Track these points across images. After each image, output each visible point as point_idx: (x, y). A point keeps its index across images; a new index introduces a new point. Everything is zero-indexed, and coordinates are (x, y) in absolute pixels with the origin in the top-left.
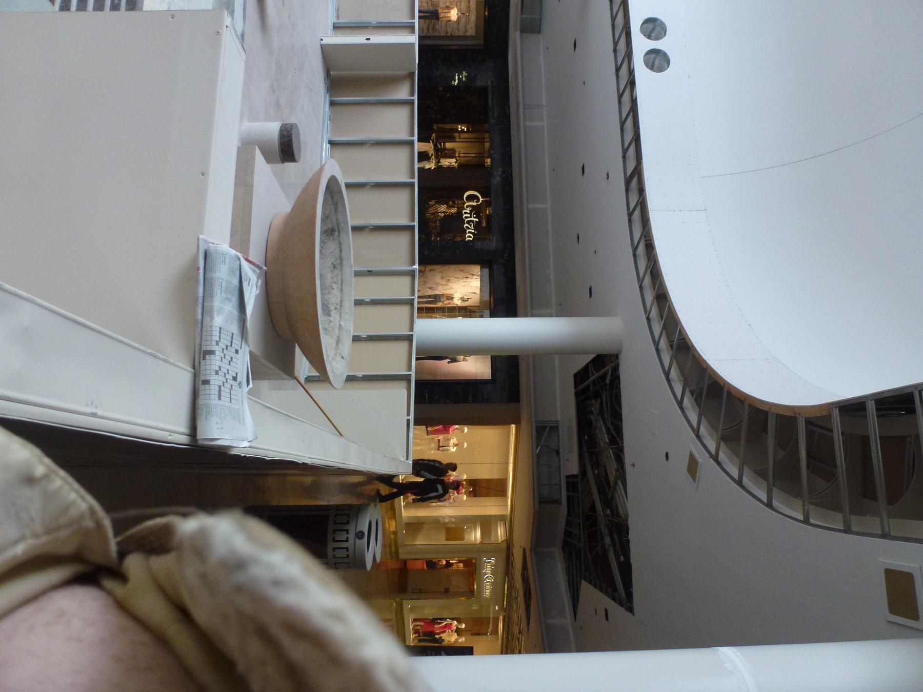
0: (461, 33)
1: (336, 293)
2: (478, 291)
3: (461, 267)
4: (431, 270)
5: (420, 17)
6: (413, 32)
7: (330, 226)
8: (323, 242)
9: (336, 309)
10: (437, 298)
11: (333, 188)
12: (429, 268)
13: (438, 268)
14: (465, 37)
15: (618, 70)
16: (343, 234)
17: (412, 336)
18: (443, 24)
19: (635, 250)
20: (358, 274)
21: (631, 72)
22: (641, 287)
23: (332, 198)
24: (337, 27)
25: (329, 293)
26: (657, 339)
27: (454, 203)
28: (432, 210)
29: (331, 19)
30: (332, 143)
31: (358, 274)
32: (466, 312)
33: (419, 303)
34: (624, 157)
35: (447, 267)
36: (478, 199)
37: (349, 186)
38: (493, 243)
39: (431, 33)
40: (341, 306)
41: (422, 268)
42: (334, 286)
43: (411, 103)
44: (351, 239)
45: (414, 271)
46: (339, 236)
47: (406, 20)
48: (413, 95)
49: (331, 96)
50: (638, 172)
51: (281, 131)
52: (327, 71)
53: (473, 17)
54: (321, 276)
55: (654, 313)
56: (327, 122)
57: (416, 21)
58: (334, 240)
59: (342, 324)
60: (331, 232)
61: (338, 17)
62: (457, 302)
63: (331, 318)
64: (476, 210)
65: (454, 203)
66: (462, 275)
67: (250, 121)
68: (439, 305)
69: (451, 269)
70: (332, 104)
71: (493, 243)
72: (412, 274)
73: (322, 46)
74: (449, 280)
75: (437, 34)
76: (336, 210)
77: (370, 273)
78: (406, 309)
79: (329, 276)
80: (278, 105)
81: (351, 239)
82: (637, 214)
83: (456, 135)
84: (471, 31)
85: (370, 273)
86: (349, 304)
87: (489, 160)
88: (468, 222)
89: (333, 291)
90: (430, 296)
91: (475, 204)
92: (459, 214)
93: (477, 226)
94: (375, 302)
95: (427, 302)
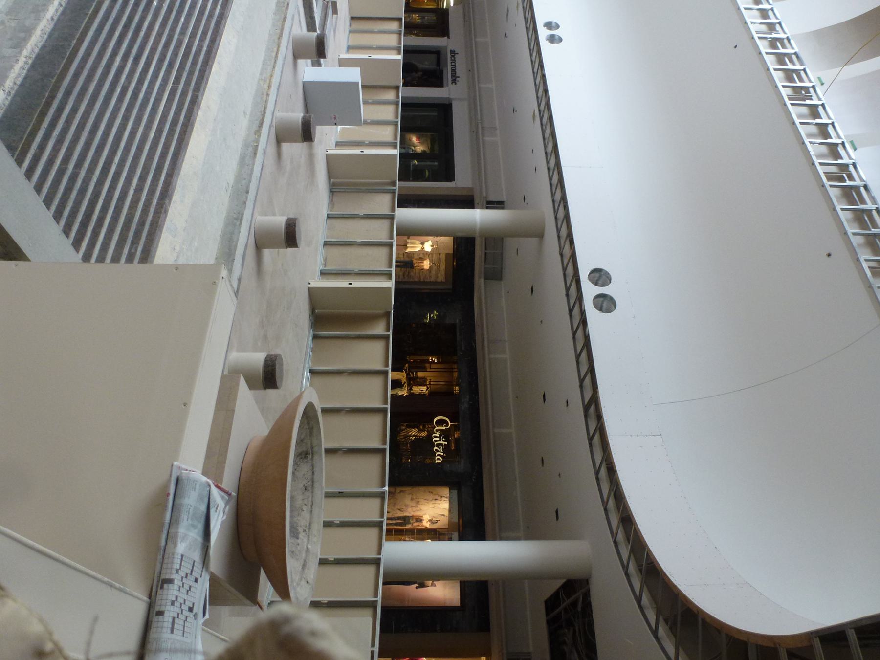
0: (432, 280)
1: (306, 515)
2: (447, 513)
3: (431, 489)
4: (401, 492)
5: (396, 266)
6: (390, 278)
7: (304, 449)
8: (296, 464)
9: (304, 531)
10: (406, 520)
11: (309, 414)
12: (399, 489)
13: (407, 489)
14: (435, 283)
15: (571, 311)
16: (316, 457)
17: (379, 559)
18: (417, 271)
19: (597, 473)
20: (328, 495)
21: (583, 313)
22: (606, 510)
23: (308, 424)
24: (323, 274)
25: (299, 515)
26: (614, 531)
27: (424, 427)
28: (403, 434)
29: (319, 267)
30: (312, 372)
31: (328, 495)
32: (436, 534)
33: (387, 524)
34: (581, 386)
35: (416, 489)
36: (447, 424)
37: (325, 411)
38: (462, 466)
39: (406, 279)
40: (310, 528)
41: (393, 490)
42: (305, 508)
43: (386, 338)
44: (324, 462)
45: (384, 493)
46: (312, 459)
47: (384, 268)
48: (388, 331)
49: (314, 331)
50: (595, 400)
51: (266, 361)
52: (313, 310)
53: (443, 267)
54: (292, 498)
55: (621, 537)
56: (309, 354)
57: (393, 270)
58: (307, 462)
59: (309, 546)
60: (304, 455)
61: (325, 265)
62: (426, 524)
63: (299, 541)
64: (445, 434)
65: (424, 427)
66: (431, 496)
67: (238, 351)
68: (408, 527)
69: (421, 491)
70: (315, 337)
71: (462, 466)
72: (381, 495)
73: (309, 289)
74: (418, 502)
75: (411, 280)
76: (311, 433)
77: (341, 495)
78: (374, 532)
79: (299, 502)
80: (265, 337)
81: (324, 462)
82: (597, 439)
83: (427, 365)
84: (441, 277)
85: (341, 495)
86: (317, 526)
87: (457, 388)
88: (438, 445)
89: (303, 513)
90: (399, 518)
91: (444, 428)
92: (429, 437)
93: (446, 449)
94: (344, 524)
95: (397, 524)
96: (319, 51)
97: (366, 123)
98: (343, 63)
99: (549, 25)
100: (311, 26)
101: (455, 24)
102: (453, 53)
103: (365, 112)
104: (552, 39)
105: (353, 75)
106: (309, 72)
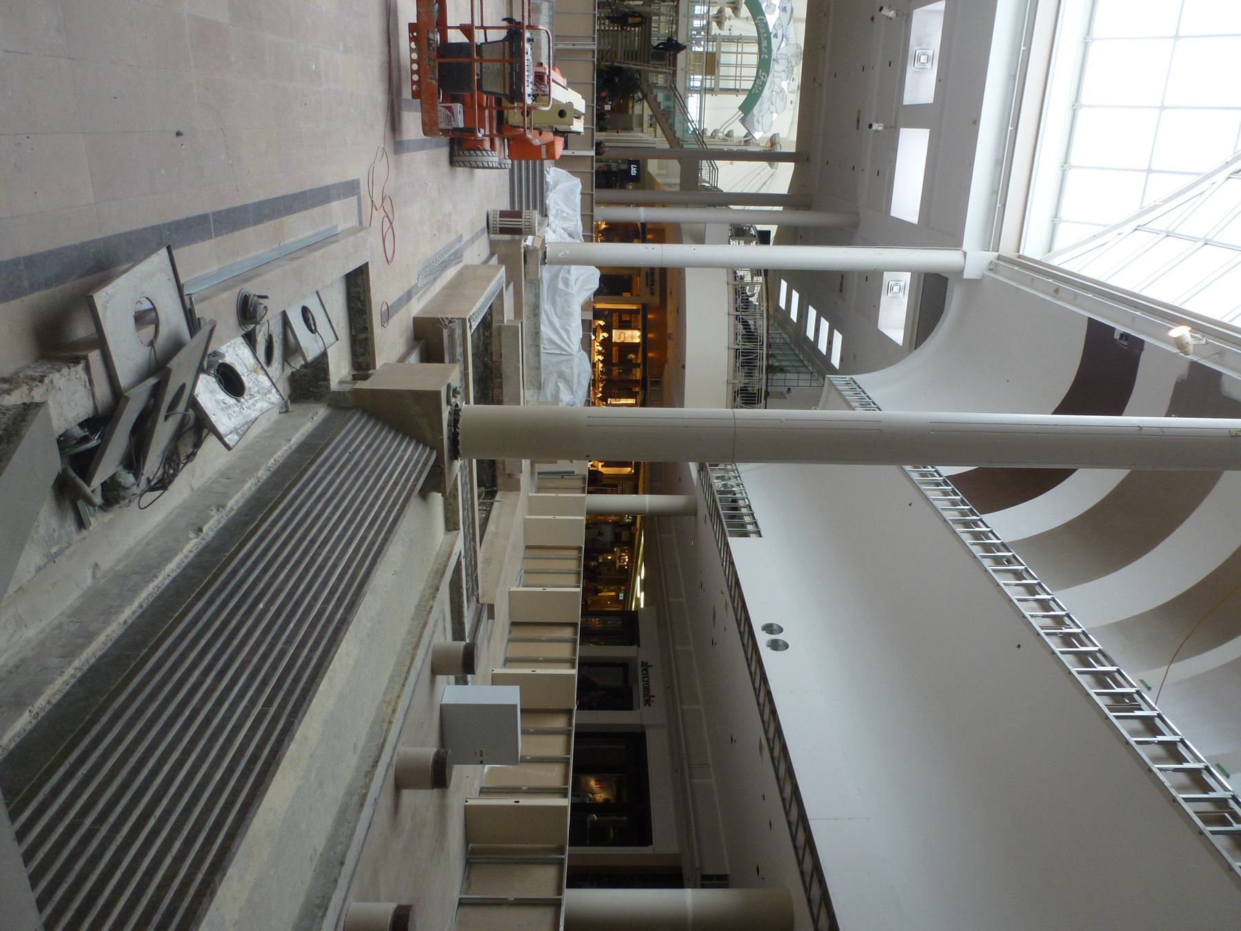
96: (466, 665)
97: (524, 760)
98: (497, 680)
99: (769, 628)
100: (458, 633)
101: (646, 629)
102: (645, 666)
103: (524, 746)
104: (775, 645)
105: (510, 695)
106: (451, 692)
